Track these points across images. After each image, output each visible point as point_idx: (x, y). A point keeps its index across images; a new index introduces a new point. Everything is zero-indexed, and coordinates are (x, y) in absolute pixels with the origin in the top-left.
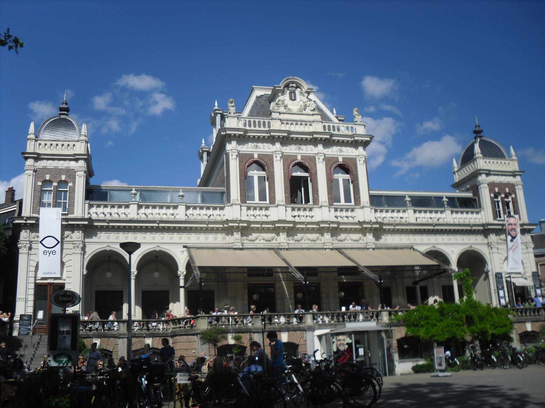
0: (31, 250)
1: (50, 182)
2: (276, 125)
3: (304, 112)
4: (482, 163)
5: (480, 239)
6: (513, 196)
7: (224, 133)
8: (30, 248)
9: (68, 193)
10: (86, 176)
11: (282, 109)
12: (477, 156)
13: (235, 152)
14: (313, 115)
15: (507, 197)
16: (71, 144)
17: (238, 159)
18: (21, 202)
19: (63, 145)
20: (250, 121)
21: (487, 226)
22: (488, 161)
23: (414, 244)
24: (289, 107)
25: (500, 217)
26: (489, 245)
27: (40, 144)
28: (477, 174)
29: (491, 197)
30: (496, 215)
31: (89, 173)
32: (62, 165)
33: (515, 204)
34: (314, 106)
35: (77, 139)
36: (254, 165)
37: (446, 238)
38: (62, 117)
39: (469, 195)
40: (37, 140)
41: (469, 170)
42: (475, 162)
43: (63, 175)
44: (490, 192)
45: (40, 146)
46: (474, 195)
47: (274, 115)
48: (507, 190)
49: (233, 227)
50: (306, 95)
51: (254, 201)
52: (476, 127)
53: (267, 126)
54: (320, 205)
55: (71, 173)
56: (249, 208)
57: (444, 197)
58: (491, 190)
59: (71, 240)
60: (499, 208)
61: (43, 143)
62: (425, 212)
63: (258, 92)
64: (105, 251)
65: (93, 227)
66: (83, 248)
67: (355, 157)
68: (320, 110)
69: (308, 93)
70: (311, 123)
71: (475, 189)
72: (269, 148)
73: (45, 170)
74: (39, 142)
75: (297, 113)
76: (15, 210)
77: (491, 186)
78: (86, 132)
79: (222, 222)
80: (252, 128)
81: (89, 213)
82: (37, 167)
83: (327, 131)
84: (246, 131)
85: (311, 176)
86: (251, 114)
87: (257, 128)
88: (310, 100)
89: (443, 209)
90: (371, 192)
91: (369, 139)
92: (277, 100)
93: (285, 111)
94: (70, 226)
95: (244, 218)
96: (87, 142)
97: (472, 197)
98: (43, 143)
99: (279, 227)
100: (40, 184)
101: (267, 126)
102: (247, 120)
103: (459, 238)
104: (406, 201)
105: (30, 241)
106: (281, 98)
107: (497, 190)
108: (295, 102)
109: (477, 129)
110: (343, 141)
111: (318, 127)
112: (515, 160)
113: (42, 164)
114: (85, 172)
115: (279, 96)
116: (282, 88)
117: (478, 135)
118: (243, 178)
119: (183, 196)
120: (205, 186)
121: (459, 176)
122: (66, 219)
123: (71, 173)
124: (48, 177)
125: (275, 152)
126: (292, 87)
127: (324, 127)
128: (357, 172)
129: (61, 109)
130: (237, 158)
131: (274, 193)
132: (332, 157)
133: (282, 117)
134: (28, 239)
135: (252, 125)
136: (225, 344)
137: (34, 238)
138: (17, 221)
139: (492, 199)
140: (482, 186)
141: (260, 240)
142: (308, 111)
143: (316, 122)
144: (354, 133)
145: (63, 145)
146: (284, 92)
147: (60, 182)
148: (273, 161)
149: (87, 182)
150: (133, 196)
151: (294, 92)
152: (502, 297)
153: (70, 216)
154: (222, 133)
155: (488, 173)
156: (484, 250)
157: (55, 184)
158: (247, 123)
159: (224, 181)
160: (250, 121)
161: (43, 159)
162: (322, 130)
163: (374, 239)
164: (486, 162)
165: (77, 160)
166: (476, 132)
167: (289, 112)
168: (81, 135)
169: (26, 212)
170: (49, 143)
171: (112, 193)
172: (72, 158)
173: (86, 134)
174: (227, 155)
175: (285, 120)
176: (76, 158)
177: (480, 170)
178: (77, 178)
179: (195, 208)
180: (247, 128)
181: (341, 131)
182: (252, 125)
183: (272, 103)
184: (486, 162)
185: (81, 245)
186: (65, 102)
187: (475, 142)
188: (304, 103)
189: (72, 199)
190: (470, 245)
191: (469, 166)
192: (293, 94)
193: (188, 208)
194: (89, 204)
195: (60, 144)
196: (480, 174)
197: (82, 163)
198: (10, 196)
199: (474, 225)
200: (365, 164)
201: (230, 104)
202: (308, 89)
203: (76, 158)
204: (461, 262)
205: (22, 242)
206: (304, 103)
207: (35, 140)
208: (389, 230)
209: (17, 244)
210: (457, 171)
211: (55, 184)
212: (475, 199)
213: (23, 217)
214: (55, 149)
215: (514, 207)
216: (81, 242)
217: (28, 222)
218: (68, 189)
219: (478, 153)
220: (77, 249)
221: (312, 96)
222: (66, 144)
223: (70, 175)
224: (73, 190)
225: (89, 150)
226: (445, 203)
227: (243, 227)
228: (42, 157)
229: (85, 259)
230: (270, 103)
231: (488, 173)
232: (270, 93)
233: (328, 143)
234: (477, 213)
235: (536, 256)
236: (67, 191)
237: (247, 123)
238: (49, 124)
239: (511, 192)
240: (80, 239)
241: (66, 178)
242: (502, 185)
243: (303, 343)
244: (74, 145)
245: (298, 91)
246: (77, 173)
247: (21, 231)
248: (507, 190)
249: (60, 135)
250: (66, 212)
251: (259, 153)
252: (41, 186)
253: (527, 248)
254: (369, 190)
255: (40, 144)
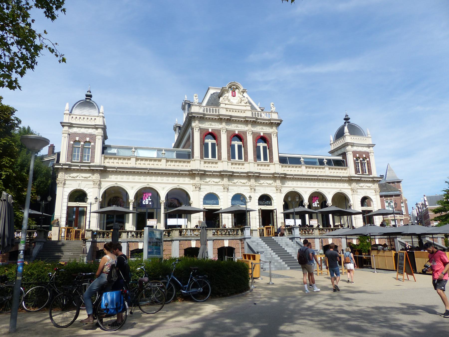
0: (65, 185)
1: (79, 142)
2: (223, 112)
3: (240, 104)
4: (348, 139)
5: (346, 185)
6: (368, 159)
7: (191, 115)
8: (64, 184)
9: (91, 149)
10: (103, 139)
11: (227, 102)
12: (346, 134)
13: (197, 128)
14: (246, 106)
15: (364, 160)
16: (93, 118)
17: (199, 132)
18: (59, 154)
19: (88, 118)
20: (207, 109)
21: (351, 178)
22: (353, 137)
23: (176, 161)
24: (231, 100)
25: (359, 172)
26: (353, 190)
27: (72, 117)
28: (346, 145)
29: (354, 160)
30: (357, 171)
31: (105, 137)
32: (87, 131)
33: (369, 165)
34: (247, 101)
35: (97, 115)
36: (209, 135)
37: (325, 185)
38: (88, 100)
39: (340, 158)
40: (71, 115)
41: (340, 143)
42: (345, 138)
43: (88, 137)
44: (354, 157)
45: (73, 119)
46: (343, 158)
47: (222, 105)
48: (364, 156)
49: (195, 173)
50: (242, 93)
51: (235, 159)
52: (346, 116)
53: (217, 112)
54: (274, 163)
55: (93, 137)
56: (232, 164)
57: (325, 159)
58: (354, 156)
59: (92, 179)
60: (359, 167)
61: (74, 117)
62: (296, 167)
63: (211, 91)
64: (176, 189)
65: (107, 171)
66: (100, 185)
67: (271, 133)
68: (250, 103)
69: (243, 92)
70: (245, 111)
71: (344, 155)
72: (218, 126)
73: (76, 134)
74: (72, 116)
75: (236, 104)
76: (55, 159)
77: (354, 153)
78: (103, 111)
79: (189, 171)
80: (208, 113)
81: (104, 162)
82: (70, 132)
83: (254, 116)
84: (204, 115)
85: (243, 143)
86: (208, 104)
87: (211, 113)
88: (244, 97)
89: (323, 166)
90: (279, 155)
91: (279, 122)
92: (224, 96)
93: (229, 103)
94: (91, 170)
95: (202, 168)
96: (103, 117)
97: (342, 159)
98: (74, 117)
99: (223, 175)
100: (72, 143)
101: (217, 112)
102: (205, 108)
103: (333, 185)
104: (301, 161)
105: (65, 179)
106: (227, 95)
107: (358, 155)
108: (235, 97)
109: (347, 117)
110: (264, 123)
111: (249, 114)
112: (370, 137)
113: (75, 130)
114: (102, 136)
115: (225, 94)
116: (227, 89)
117: (347, 121)
118: (202, 143)
119: (165, 154)
120: (177, 148)
121: (334, 146)
122: (89, 165)
123: (93, 137)
124: (77, 139)
125: (222, 128)
126: (234, 88)
127: (252, 113)
128: (272, 142)
129: (87, 96)
130: (199, 131)
131: (221, 153)
132: (256, 133)
133: (227, 106)
134: (63, 178)
135: (208, 111)
136: (190, 247)
137: (68, 177)
138: (56, 166)
139: (354, 161)
140: (348, 153)
141: (211, 182)
142: (243, 104)
143: (247, 110)
144: (271, 118)
145: (88, 118)
146: (228, 91)
147: (86, 142)
148: (221, 134)
149: (103, 143)
150: (133, 152)
151: (234, 91)
152: (420, 242)
153: (92, 164)
154: (190, 115)
155: (353, 145)
156: (348, 193)
157: (82, 143)
158: (205, 110)
159: (190, 145)
160: (207, 109)
161: (74, 127)
162: (251, 116)
163: (281, 184)
164: (351, 138)
165: (97, 128)
166: (345, 119)
167: (231, 104)
168: (99, 113)
169: (63, 160)
170: (78, 117)
171: (119, 151)
172: (94, 127)
173: (103, 112)
174: (192, 129)
175: (240, 110)
176: (96, 127)
177: (347, 143)
178: (97, 140)
179: (172, 161)
180: (205, 113)
181: (262, 116)
182: (208, 111)
183: (221, 98)
184: (351, 138)
185: (99, 183)
186: (89, 91)
187: (345, 125)
188: (240, 98)
189: (93, 153)
190: (340, 189)
191: (341, 140)
192: (234, 92)
193: (167, 161)
194: (104, 157)
195: (86, 117)
196: (348, 145)
197: (100, 131)
198: (51, 150)
199: (343, 177)
200: (276, 137)
201: (195, 98)
202: (243, 90)
203: (96, 127)
204: (333, 199)
205: (59, 180)
206: (240, 98)
207: (69, 114)
208: (290, 178)
209: (56, 181)
210: (333, 143)
211: (82, 143)
212: (344, 161)
213: (60, 164)
214: (82, 121)
215: (368, 166)
216: (98, 181)
217: (63, 167)
218: (91, 147)
219: (347, 132)
220: (96, 185)
221: (245, 94)
222: (90, 118)
223: (92, 138)
224: (94, 147)
225: (105, 123)
226: (325, 163)
227: (201, 174)
228: (74, 125)
229: (100, 192)
230: (219, 98)
231: (353, 145)
232: (219, 91)
233: (255, 123)
234: (345, 169)
235: (381, 196)
236: (90, 148)
237: (205, 110)
238: (78, 104)
239: (367, 157)
240: (98, 179)
241: (89, 140)
242: (361, 153)
243: (237, 247)
244: (95, 119)
245: (237, 91)
246: (97, 137)
247: (58, 173)
248: (364, 156)
249: (86, 111)
250: (90, 162)
251: (238, 130)
252: (73, 144)
253: (376, 192)
254: (279, 154)
255: (72, 117)
